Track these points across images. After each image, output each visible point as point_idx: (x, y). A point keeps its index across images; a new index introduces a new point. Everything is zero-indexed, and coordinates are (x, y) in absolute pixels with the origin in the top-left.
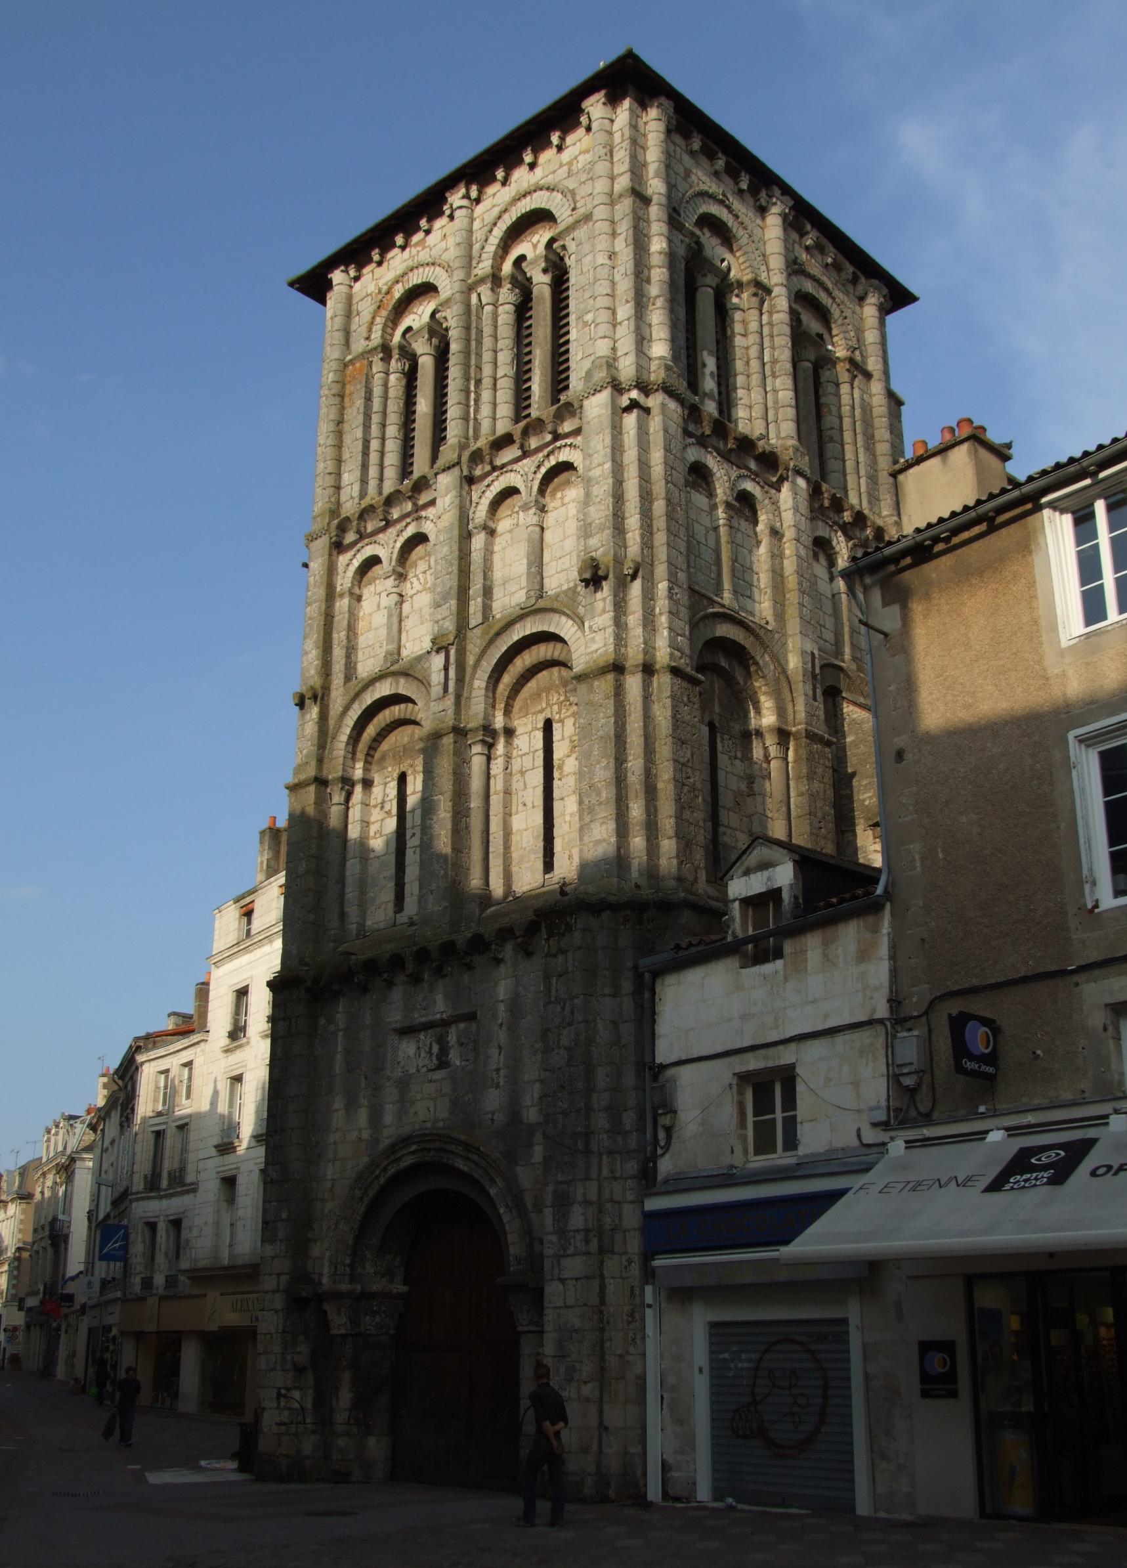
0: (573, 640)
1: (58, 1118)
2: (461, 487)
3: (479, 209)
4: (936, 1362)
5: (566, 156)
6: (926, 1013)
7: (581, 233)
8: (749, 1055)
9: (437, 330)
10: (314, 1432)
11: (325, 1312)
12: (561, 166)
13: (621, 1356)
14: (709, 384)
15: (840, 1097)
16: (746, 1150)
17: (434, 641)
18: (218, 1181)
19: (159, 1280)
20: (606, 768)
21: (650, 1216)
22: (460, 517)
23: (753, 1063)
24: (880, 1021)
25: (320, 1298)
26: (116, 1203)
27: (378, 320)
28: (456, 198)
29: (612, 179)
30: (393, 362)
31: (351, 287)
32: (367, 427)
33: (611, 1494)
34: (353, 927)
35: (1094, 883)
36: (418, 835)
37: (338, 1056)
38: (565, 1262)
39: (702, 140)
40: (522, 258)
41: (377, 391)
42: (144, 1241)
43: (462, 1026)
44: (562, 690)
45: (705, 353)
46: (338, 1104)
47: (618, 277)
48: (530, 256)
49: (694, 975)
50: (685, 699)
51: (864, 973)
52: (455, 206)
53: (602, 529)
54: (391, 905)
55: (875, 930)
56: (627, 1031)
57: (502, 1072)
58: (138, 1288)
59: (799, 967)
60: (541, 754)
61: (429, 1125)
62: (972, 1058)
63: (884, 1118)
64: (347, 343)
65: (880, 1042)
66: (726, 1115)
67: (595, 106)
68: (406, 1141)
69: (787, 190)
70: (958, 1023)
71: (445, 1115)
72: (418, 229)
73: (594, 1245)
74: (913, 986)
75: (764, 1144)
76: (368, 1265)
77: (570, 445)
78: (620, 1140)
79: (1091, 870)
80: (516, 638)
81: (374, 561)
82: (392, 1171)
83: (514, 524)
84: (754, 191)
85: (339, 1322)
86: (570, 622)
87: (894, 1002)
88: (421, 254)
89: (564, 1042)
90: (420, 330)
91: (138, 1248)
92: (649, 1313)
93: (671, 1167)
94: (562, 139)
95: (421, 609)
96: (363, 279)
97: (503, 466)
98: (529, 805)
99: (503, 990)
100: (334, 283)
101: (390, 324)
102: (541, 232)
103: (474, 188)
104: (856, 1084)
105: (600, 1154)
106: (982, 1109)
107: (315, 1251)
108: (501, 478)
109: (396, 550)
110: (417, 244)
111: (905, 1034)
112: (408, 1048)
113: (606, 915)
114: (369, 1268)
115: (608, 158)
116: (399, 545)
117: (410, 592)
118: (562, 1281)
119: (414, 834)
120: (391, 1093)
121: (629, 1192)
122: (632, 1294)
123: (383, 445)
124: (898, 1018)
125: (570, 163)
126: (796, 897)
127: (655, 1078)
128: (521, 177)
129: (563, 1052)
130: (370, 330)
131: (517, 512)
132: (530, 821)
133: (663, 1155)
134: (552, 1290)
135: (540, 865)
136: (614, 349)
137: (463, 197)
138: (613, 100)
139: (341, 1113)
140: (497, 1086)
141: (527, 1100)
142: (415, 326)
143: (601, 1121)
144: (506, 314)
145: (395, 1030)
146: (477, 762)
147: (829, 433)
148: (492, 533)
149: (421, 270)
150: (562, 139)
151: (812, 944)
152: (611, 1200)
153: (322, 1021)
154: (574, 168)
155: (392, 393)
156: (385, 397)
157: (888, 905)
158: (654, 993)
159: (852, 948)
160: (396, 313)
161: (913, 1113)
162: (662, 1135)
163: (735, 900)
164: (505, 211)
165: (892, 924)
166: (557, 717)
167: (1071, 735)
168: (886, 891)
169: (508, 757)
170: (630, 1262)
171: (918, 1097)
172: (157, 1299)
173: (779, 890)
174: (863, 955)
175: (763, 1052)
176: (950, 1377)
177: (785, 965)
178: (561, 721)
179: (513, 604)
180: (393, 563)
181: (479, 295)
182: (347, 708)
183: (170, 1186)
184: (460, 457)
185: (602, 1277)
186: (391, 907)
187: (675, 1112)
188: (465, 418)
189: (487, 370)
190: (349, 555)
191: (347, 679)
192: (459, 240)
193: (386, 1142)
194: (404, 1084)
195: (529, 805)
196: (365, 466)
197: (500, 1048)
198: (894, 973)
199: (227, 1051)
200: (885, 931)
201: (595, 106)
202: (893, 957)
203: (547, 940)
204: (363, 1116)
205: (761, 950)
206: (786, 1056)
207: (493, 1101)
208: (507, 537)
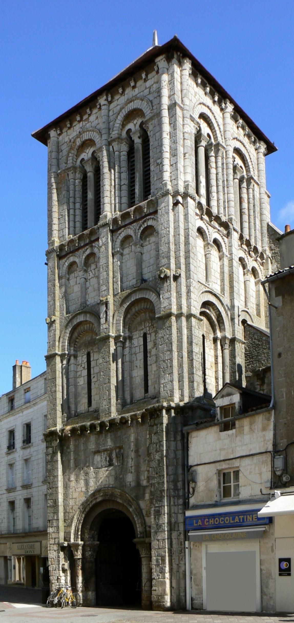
0: (155, 301)
3: (112, 105)
5: (148, 84)
6: (285, 449)
8: (223, 463)
11: (72, 551)
12: (146, 88)
13: (178, 565)
16: (220, 496)
18: (8, 503)
23: (224, 466)
24: (270, 452)
28: (102, 101)
30: (77, 174)
31: (58, 138)
34: (73, 412)
36: (96, 377)
37: (72, 461)
39: (218, 96)
44: (150, 321)
48: (133, 129)
51: (264, 435)
52: (101, 104)
55: (269, 419)
56: (180, 453)
57: (133, 468)
59: (241, 432)
60: (142, 347)
64: (58, 165)
65: (269, 459)
66: (214, 483)
71: (113, 483)
74: (281, 440)
77: (153, 218)
78: (176, 492)
80: (133, 300)
81: (74, 263)
82: (94, 502)
86: (154, 294)
87: (275, 445)
88: (87, 125)
90: (88, 160)
93: (194, 501)
94: (147, 75)
95: (94, 285)
96: (63, 135)
98: (139, 367)
100: (51, 136)
101: (75, 157)
102: (137, 119)
103: (110, 96)
104: (260, 474)
108: (125, 231)
109: (83, 260)
110: (85, 120)
111: (278, 457)
116: (84, 257)
117: (89, 278)
118: (158, 540)
119: (94, 377)
121: (180, 510)
122: (181, 544)
124: (276, 451)
125: (150, 88)
126: (240, 407)
127: (188, 470)
128: (129, 93)
130: (67, 160)
131: (131, 246)
132: (139, 373)
133: (191, 497)
135: (143, 390)
137: (105, 100)
140: (132, 472)
141: (142, 478)
142: (86, 158)
149: (88, 133)
150: (147, 75)
151: (246, 422)
152: (174, 513)
153: (65, 448)
154: (151, 90)
155: (77, 189)
158: (188, 440)
159: (260, 426)
161: (280, 484)
162: (191, 490)
163: (218, 407)
164: (123, 108)
165: (275, 418)
166: (148, 332)
168: (273, 406)
169: (130, 348)
170: (180, 533)
173: (234, 404)
174: (264, 429)
175: (227, 462)
177: (236, 431)
178: (150, 334)
179: (131, 285)
180: (82, 265)
181: (113, 147)
186: (86, 405)
190: (64, 260)
192: (104, 120)
193: (91, 492)
195: (139, 367)
197: (132, 459)
198: (275, 435)
199: (8, 454)
202: (275, 429)
203: (150, 420)
204: (82, 482)
207: (130, 478)
208: (127, 256)
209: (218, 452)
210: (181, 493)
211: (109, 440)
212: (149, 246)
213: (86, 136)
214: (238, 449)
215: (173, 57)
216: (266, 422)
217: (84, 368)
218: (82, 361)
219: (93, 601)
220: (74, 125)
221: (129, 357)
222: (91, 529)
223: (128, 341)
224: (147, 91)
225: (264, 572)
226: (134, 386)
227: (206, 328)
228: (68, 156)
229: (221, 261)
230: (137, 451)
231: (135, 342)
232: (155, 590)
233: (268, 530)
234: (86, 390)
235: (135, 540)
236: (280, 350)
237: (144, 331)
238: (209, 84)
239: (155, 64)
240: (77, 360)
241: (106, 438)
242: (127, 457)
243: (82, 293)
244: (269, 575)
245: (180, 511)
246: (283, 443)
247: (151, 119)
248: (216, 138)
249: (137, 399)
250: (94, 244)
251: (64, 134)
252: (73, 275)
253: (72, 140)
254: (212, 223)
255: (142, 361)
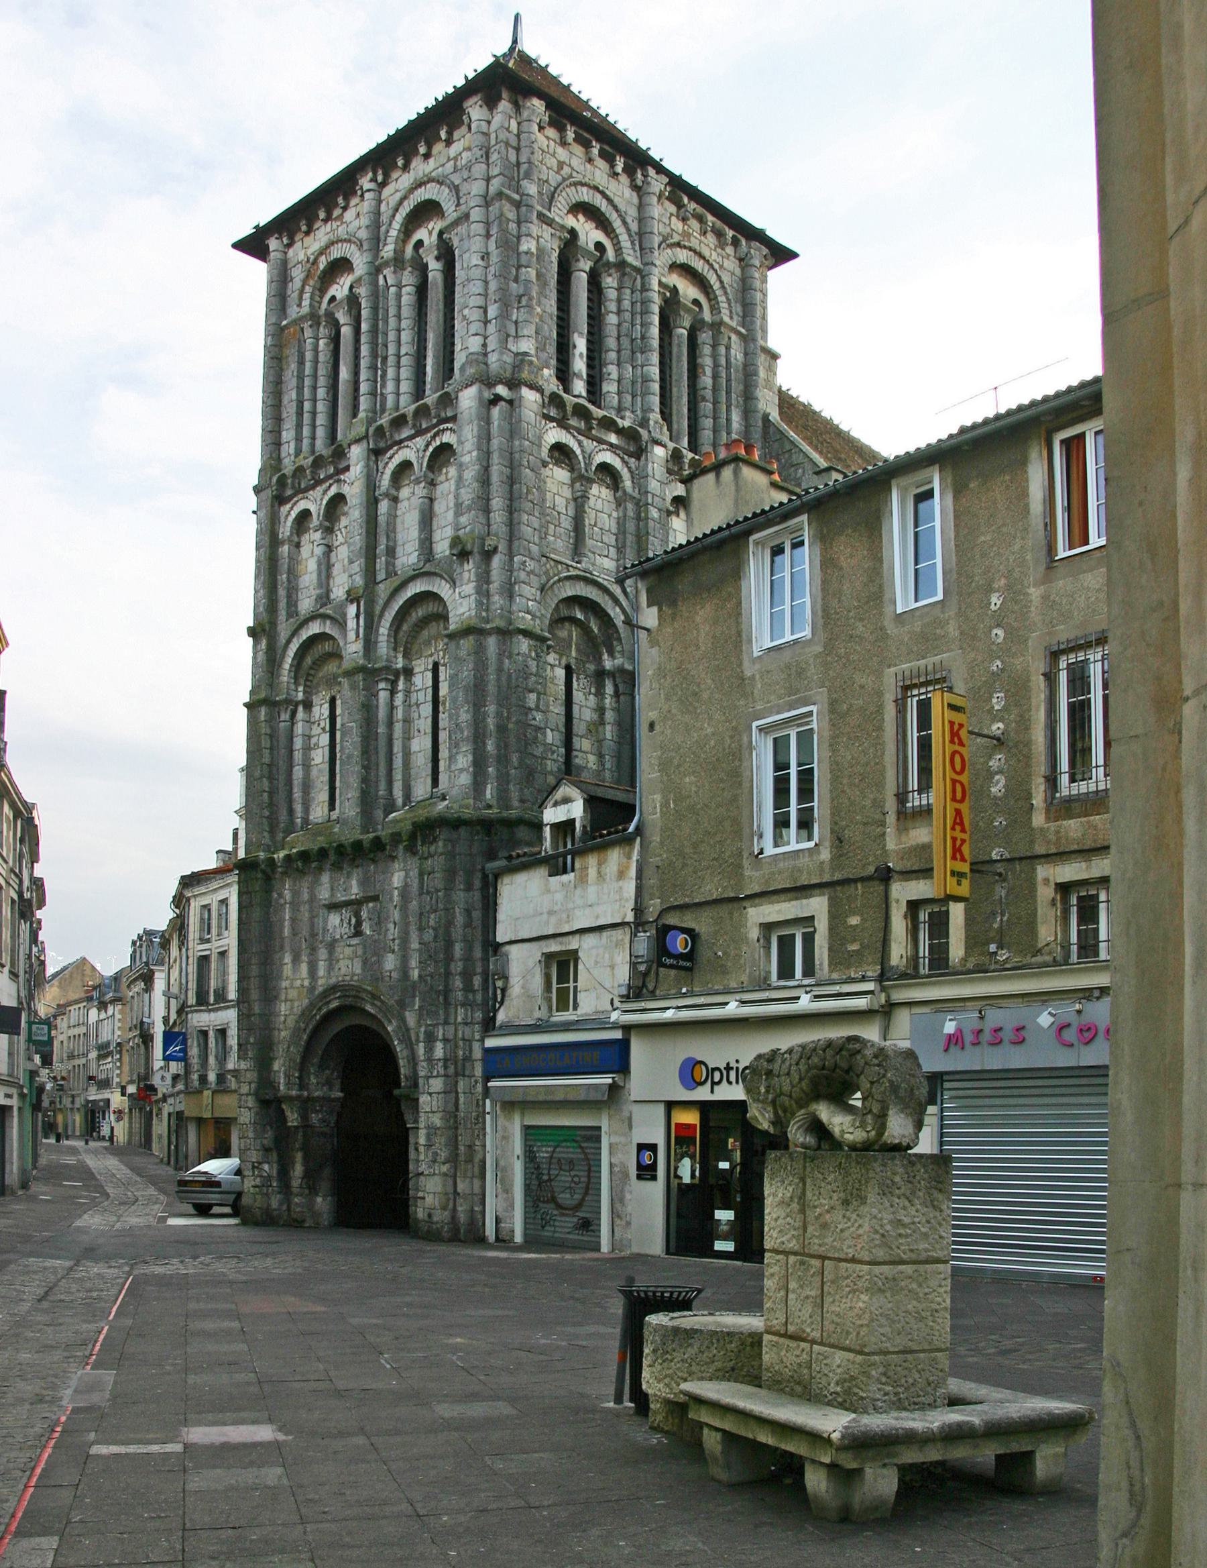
1: (141, 932)
2: (368, 459)
3: (387, 191)
4: (647, 1158)
7: (462, 229)
8: (551, 941)
9: (353, 301)
10: (279, 1193)
12: (449, 160)
14: (579, 365)
15: (604, 973)
16: (550, 1008)
17: (348, 593)
19: (212, 1077)
20: (467, 711)
21: (488, 1051)
22: (368, 486)
23: (554, 947)
24: (628, 923)
25: (279, 1101)
26: (180, 1012)
27: (308, 289)
29: (488, 180)
30: (321, 329)
32: (300, 388)
33: (462, 1236)
35: (761, 836)
38: (432, 1081)
40: (420, 243)
41: (309, 356)
42: (199, 1045)
43: (371, 905)
45: (576, 335)
46: (288, 959)
47: (490, 277)
48: (426, 243)
49: (521, 878)
50: (533, 654)
53: (469, 509)
54: (326, 804)
57: (397, 942)
58: (196, 1083)
59: (583, 880)
60: (430, 691)
61: (348, 978)
62: (670, 956)
63: (625, 993)
66: (537, 981)
67: (475, 110)
68: (334, 988)
69: (660, 169)
70: (664, 931)
72: (337, 205)
73: (451, 1070)
75: (563, 1005)
76: (312, 1077)
79: (759, 826)
83: (411, 496)
84: (629, 171)
85: (293, 1118)
87: (638, 910)
89: (432, 923)
90: (342, 301)
91: (194, 1051)
92: (488, 1117)
94: (450, 133)
97: (401, 441)
99: (397, 879)
100: (271, 249)
101: (317, 293)
104: (612, 967)
105: (456, 1006)
106: (684, 990)
107: (276, 1066)
108: (400, 452)
110: (337, 219)
112: (334, 919)
113: (463, 832)
114: (313, 1080)
115: (484, 160)
116: (324, 502)
117: (336, 544)
118: (430, 1094)
120: (323, 953)
123: (315, 406)
124: (639, 923)
125: (455, 159)
127: (495, 952)
128: (420, 168)
129: (431, 931)
134: (423, 1099)
136: (484, 345)
137: (371, 181)
138: (491, 103)
139: (290, 966)
140: (393, 952)
142: (339, 296)
143: (458, 983)
144: (408, 296)
145: (324, 905)
146: (383, 696)
147: (702, 392)
148: (395, 500)
151: (592, 860)
153: (275, 895)
154: (458, 163)
155: (321, 358)
156: (316, 361)
157: (638, 839)
158: (496, 889)
160: (322, 283)
167: (755, 724)
168: (637, 828)
169: (408, 693)
170: (476, 1082)
171: (648, 980)
172: (210, 1092)
176: (653, 1167)
181: (385, 277)
182: (289, 641)
183: (216, 1002)
184: (367, 430)
185: (457, 1093)
186: (326, 809)
187: (507, 978)
188: (373, 393)
189: (392, 349)
190: (288, 506)
191: (289, 616)
194: (331, 946)
196: (299, 426)
200: (635, 858)
201: (475, 110)
202: (639, 876)
204: (304, 968)
205: (557, 865)
206: (573, 943)
209: (545, 916)
210: (479, 997)
211: (354, 883)
212: (447, 484)
213: (336, 253)
214: (578, 913)
215: (500, 98)
216: (625, 860)
217: (323, 729)
218: (321, 714)
219: (326, 1219)
220: (316, 227)
221: (404, 711)
222: (321, 1067)
223: (402, 678)
224: (450, 166)
225: (616, 1169)
226: (412, 772)
227: (578, 650)
228: (302, 292)
229: (621, 509)
230: (404, 909)
231: (417, 680)
232: (424, 1198)
233: (621, 1084)
234: (326, 778)
235: (396, 1092)
236: (653, 715)
237: (435, 658)
238: (597, 140)
239: (463, 111)
240: (310, 711)
241: (348, 878)
242: (387, 919)
243: (319, 575)
244: (626, 1175)
245: (477, 1037)
246: (654, 906)
247: (456, 223)
248: (618, 249)
249: (419, 799)
250: (342, 477)
251: (298, 245)
252: (307, 536)
253: (312, 257)
254: (594, 432)
255: (430, 720)
